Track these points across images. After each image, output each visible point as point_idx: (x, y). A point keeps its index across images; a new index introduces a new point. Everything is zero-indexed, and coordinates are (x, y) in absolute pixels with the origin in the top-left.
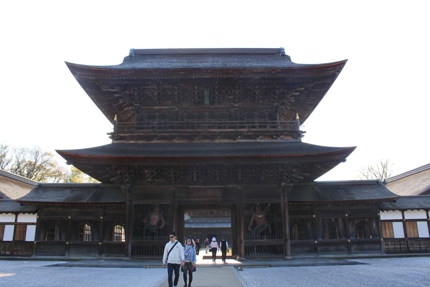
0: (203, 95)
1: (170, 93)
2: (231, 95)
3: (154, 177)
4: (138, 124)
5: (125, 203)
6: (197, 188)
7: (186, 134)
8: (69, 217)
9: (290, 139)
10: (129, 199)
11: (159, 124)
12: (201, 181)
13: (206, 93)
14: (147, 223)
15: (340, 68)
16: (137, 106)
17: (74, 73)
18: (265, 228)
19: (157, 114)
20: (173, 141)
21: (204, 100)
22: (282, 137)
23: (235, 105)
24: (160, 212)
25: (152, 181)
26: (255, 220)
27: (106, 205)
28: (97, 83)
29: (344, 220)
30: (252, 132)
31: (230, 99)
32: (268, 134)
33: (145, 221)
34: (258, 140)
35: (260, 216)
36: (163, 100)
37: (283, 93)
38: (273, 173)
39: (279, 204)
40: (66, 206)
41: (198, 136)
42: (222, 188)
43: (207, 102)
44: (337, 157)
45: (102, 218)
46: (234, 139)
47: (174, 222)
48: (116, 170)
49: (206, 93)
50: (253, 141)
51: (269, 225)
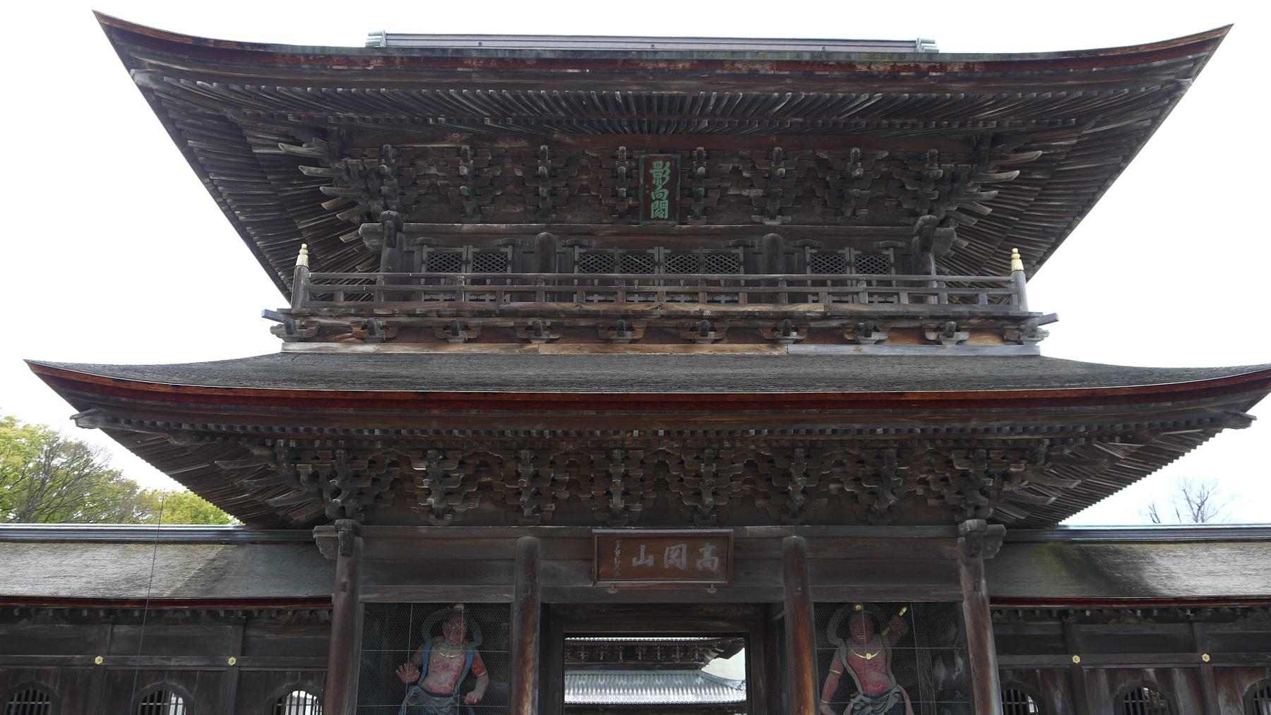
0: (649, 178)
1: (519, 173)
2: (752, 186)
3: (449, 493)
4: (391, 280)
5: (327, 600)
6: (626, 538)
7: (583, 323)
8: (99, 660)
9: (992, 347)
10: (344, 580)
11: (475, 281)
12: (637, 508)
13: (660, 171)
14: (415, 683)
15: (1196, 61)
16: (391, 217)
17: (130, 63)
18: (891, 704)
19: (468, 252)
20: (530, 347)
21: (648, 201)
22: (963, 336)
23: (768, 223)
24: (469, 637)
25: (442, 506)
26: (845, 672)
27: (254, 608)
28: (229, 113)
29: (1195, 676)
30: (840, 317)
31: (748, 200)
32: (905, 324)
33: (408, 674)
34: (867, 349)
35: (869, 656)
36: (493, 201)
37: (954, 178)
38: (924, 482)
39: (952, 609)
40: (85, 613)
41: (631, 328)
42: (726, 537)
43: (660, 208)
44: (1212, 407)
45: (232, 661)
46: (774, 343)
47: (984, 581)
48: (295, 457)
49: (660, 171)
50: (849, 350)
51: (905, 694)
